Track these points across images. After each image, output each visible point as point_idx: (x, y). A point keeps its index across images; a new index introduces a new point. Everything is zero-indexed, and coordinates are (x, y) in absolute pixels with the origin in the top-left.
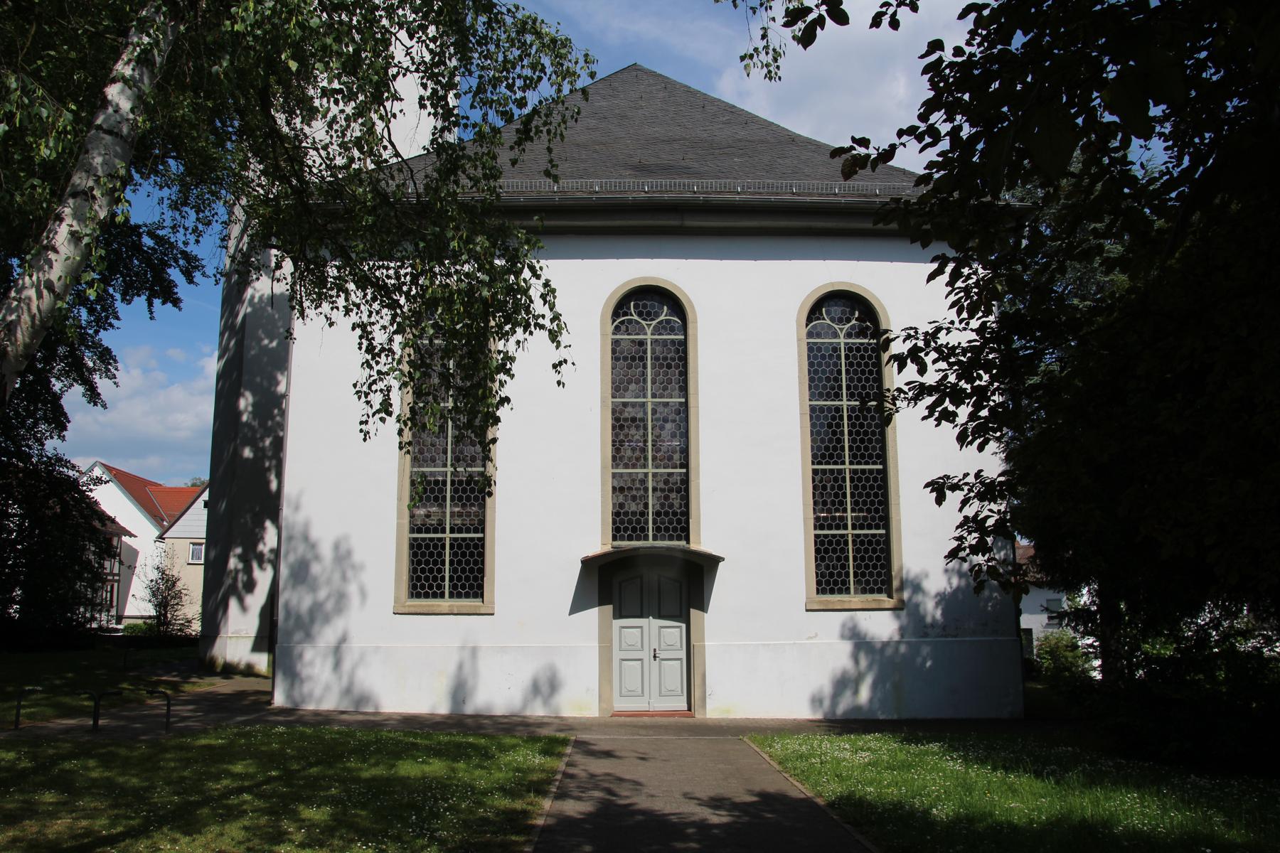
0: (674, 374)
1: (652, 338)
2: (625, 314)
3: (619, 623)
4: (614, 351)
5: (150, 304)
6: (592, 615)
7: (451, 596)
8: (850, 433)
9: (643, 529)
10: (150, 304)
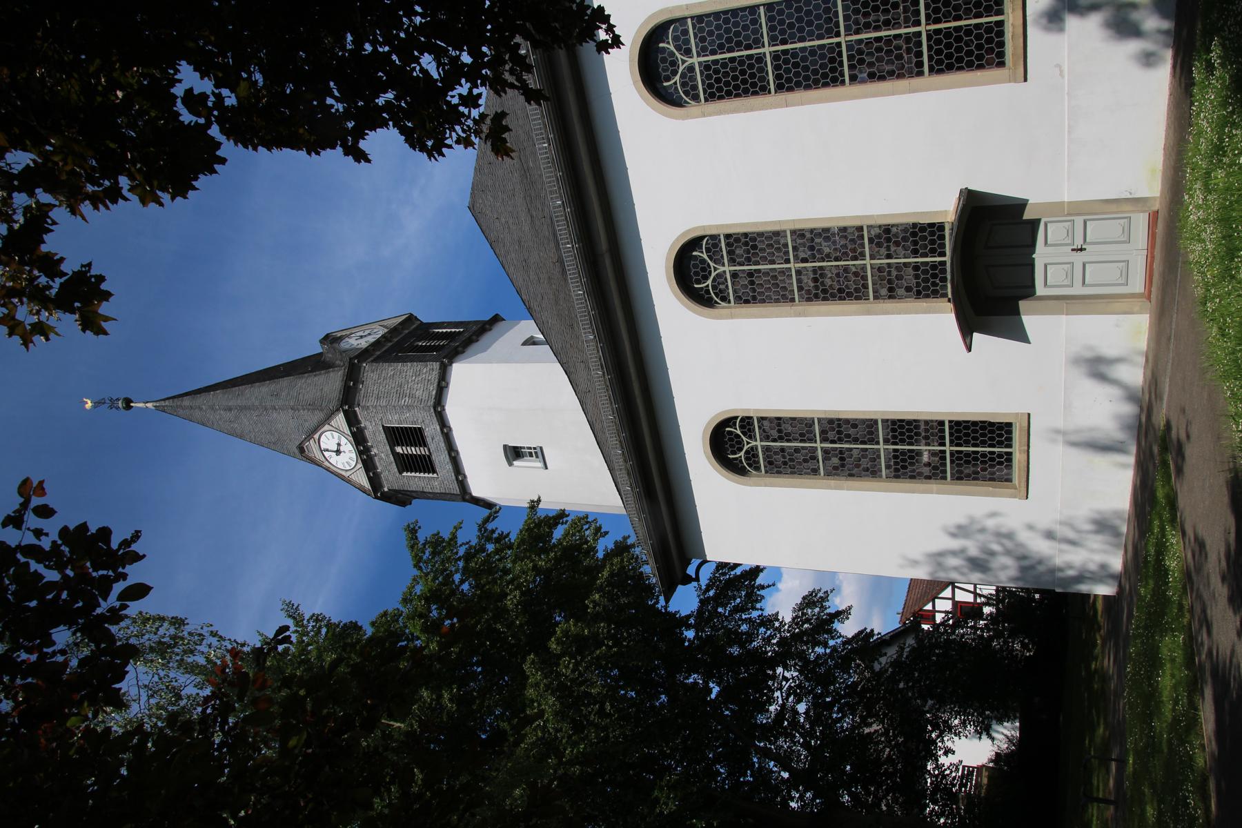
1: (724, 269)
2: (708, 292)
3: (1040, 290)
4: (747, 302)
5: (763, 587)
6: (1030, 321)
7: (1010, 446)
8: (802, 40)
9: (934, 266)
10: (763, 587)
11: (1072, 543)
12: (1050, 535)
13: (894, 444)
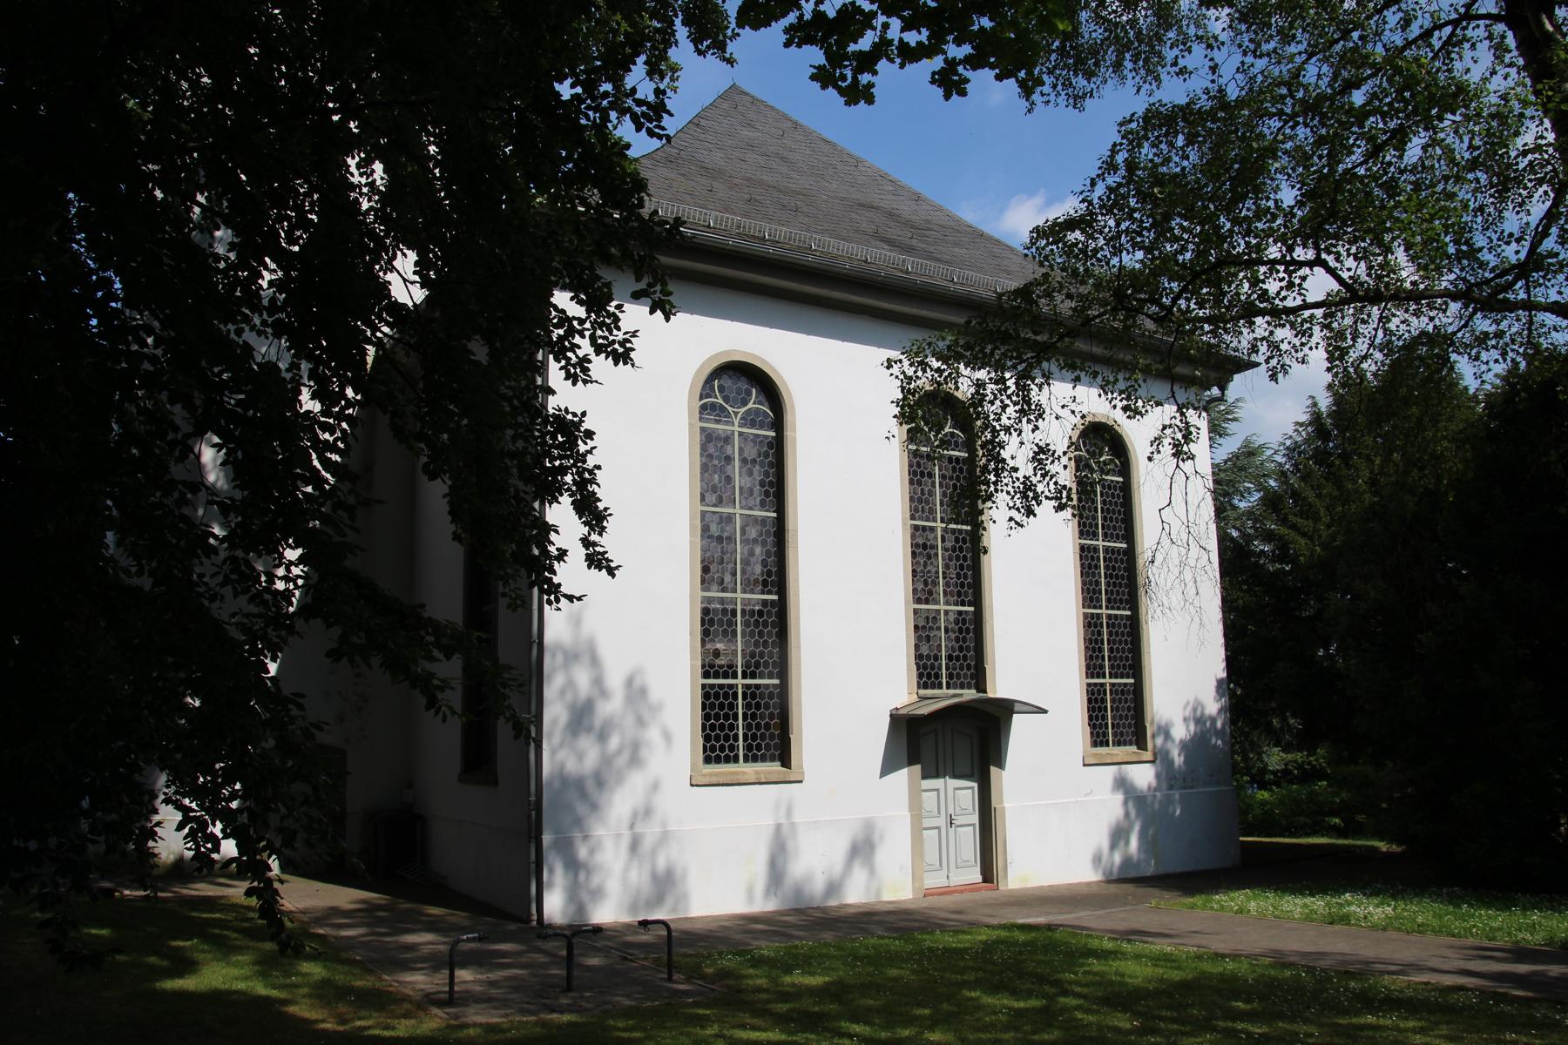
0: (770, 631)
6: (902, 776)
7: (746, 760)
9: (938, 676)
11: (635, 845)
12: (645, 812)
13: (743, 611)
